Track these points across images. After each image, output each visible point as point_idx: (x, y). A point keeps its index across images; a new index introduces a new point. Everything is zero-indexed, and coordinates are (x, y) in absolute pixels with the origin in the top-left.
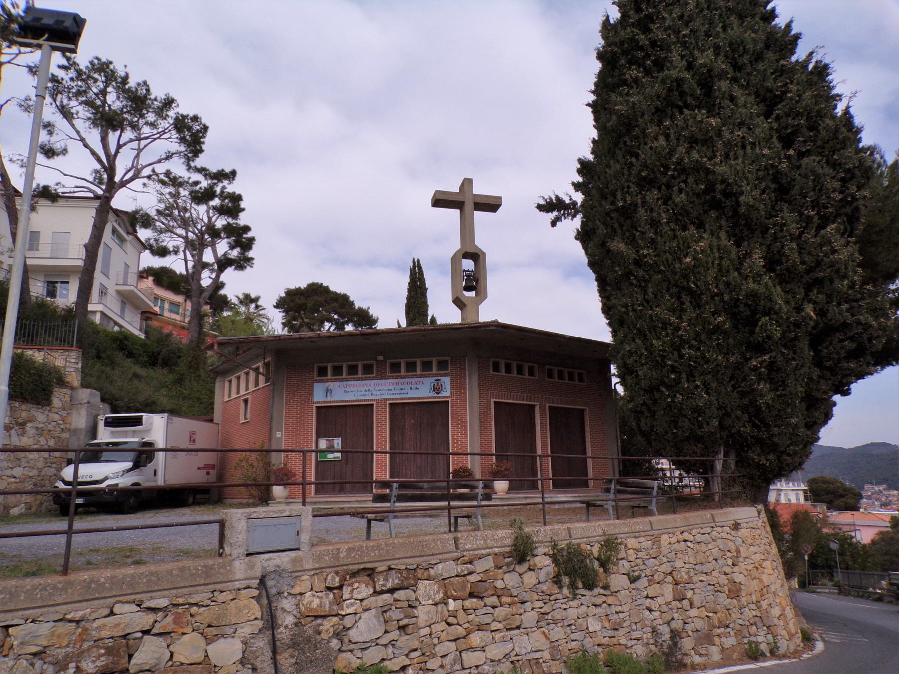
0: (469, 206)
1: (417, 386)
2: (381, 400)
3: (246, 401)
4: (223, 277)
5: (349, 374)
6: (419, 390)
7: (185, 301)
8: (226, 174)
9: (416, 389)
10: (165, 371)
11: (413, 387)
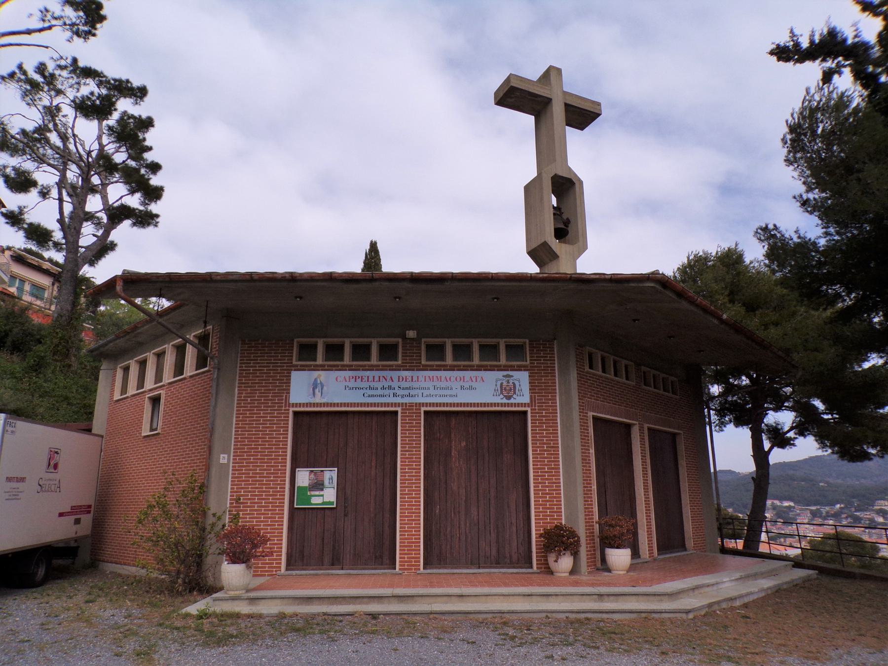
0: (558, 111)
1: (474, 385)
2: (411, 405)
3: (155, 401)
4: (115, 235)
5: (355, 357)
6: (478, 389)
7: (53, 284)
9: (471, 388)
10: (15, 358)
11: (466, 385)
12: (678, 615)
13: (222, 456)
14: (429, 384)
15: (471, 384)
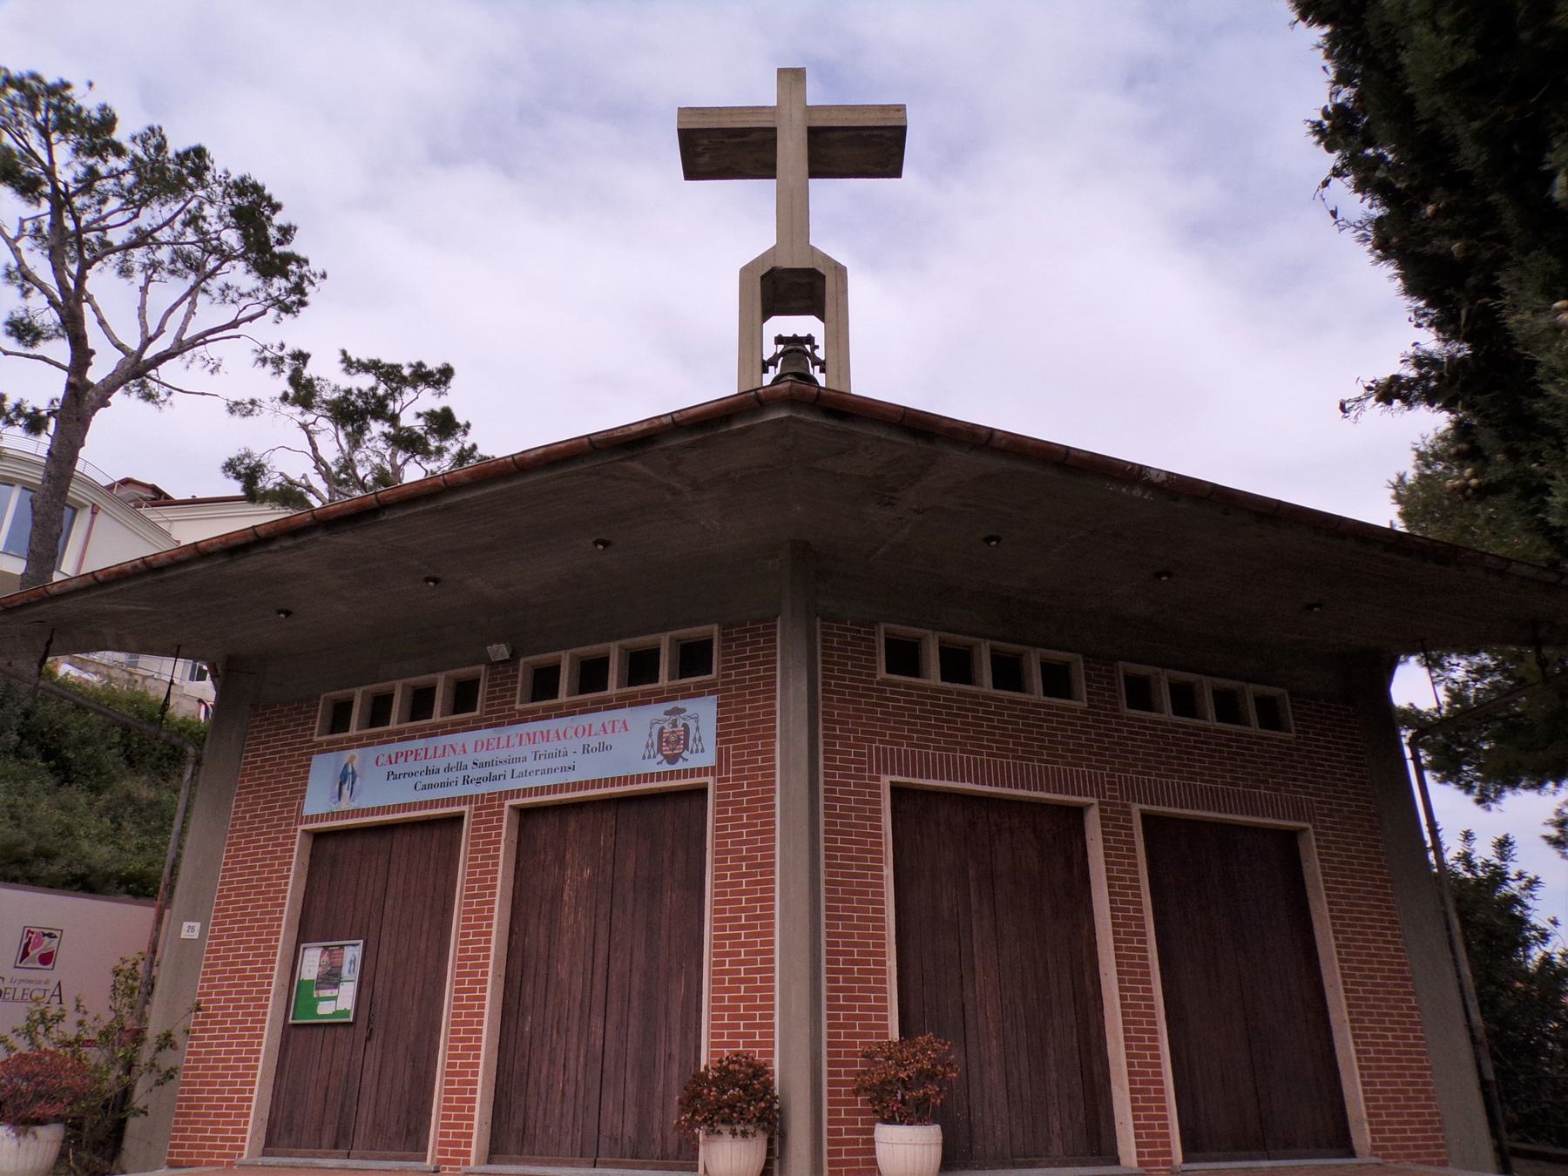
1: (608, 739)
8: (430, 374)
9: (603, 747)
13: (186, 925)
14: (527, 750)
15: (602, 737)
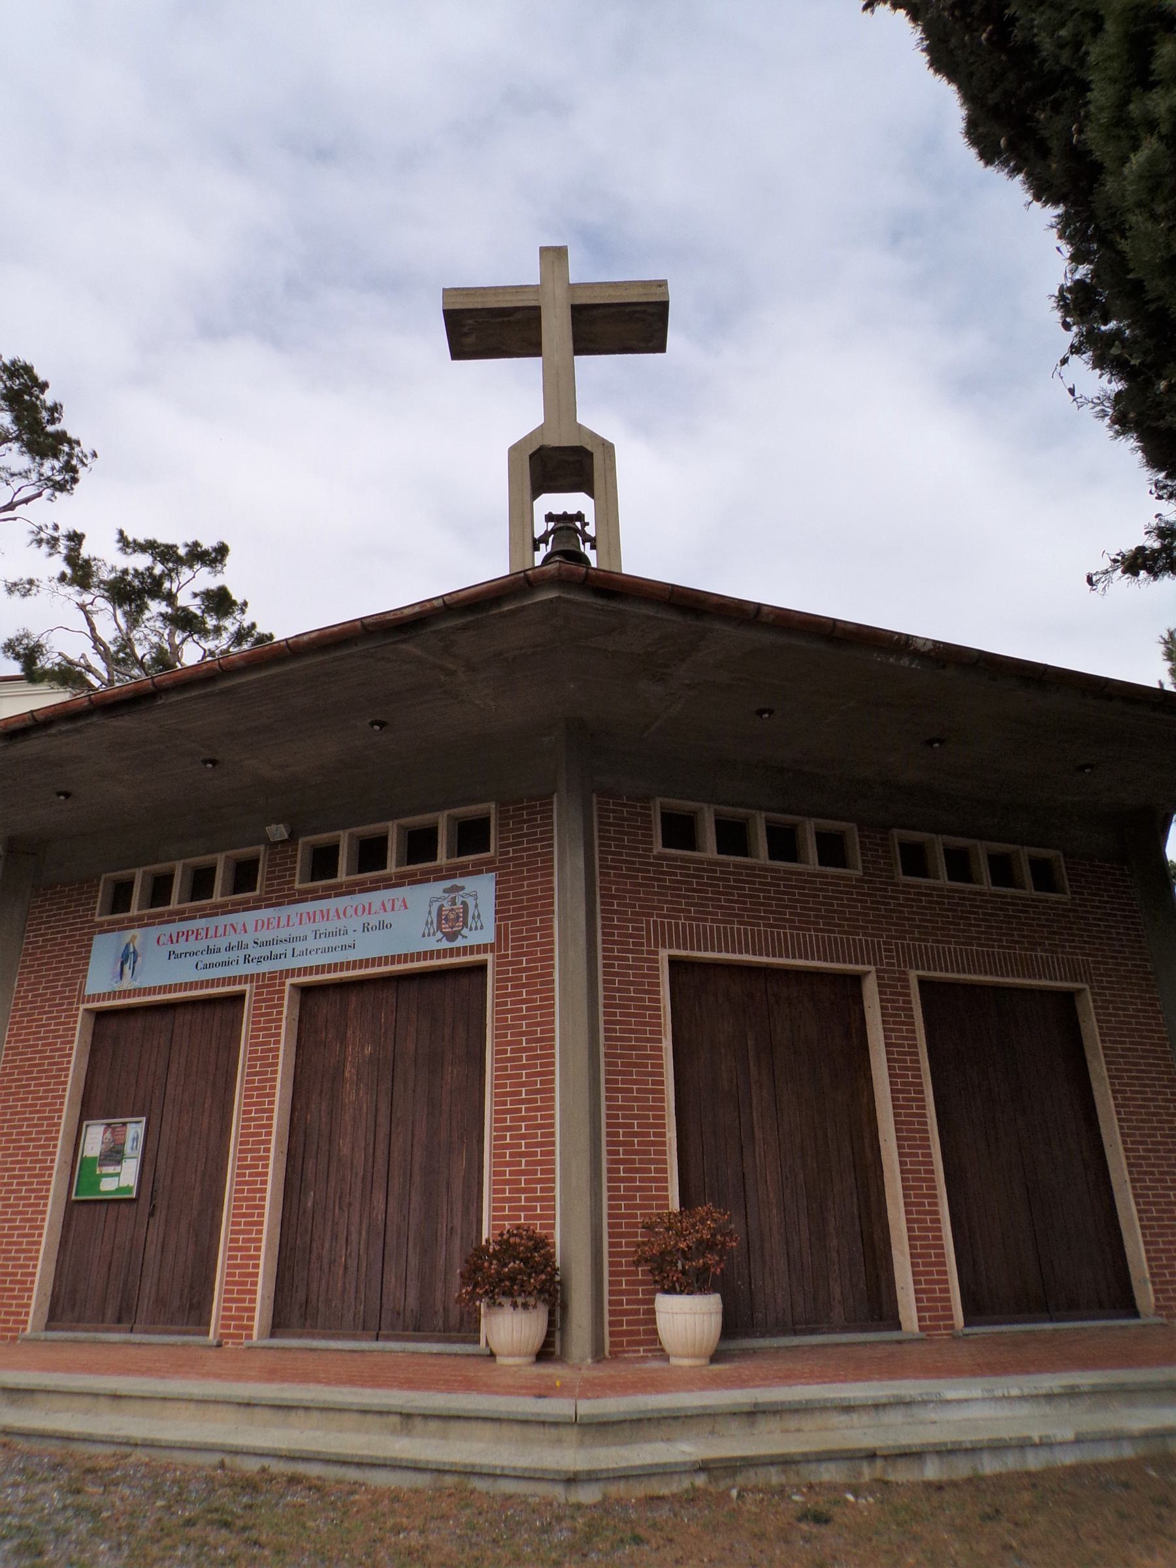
1: (388, 917)
8: (206, 553)
9: (382, 926)
12: (543, 1489)
14: (307, 929)
15: (382, 916)
